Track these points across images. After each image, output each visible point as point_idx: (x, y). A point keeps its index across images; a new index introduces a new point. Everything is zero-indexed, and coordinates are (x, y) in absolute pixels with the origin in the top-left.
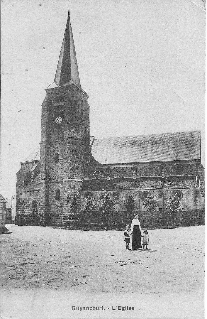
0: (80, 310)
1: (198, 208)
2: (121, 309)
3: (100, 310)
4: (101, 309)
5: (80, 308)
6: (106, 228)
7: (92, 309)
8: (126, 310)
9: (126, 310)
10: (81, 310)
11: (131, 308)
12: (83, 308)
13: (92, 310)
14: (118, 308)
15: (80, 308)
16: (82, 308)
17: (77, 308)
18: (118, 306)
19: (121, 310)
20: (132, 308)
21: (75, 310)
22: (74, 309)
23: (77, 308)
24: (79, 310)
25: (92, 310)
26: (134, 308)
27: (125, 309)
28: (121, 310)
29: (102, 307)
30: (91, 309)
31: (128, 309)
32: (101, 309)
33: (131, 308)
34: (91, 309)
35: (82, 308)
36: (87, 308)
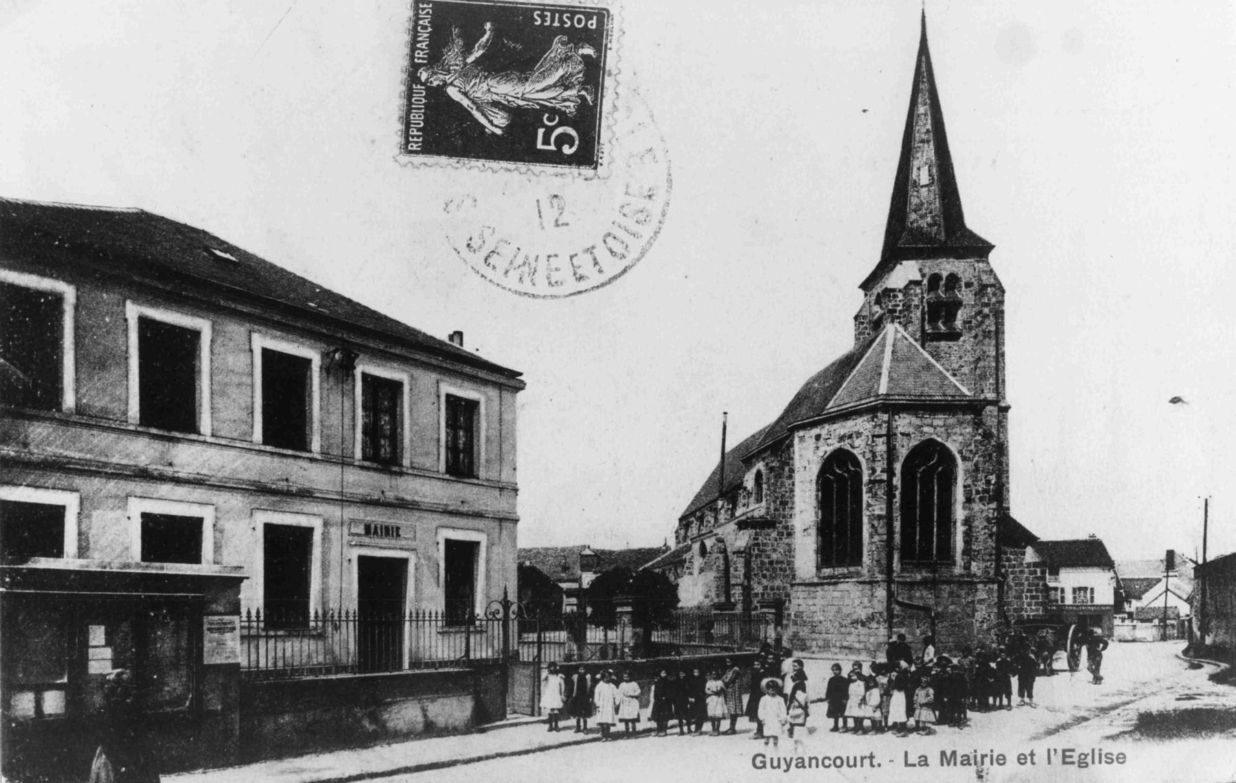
0: (784, 767)
1: (340, 386)
2: (1075, 759)
3: (862, 766)
4: (867, 762)
5: (785, 759)
6: (1098, 659)
7: (832, 762)
8: (1093, 763)
9: (1093, 763)
10: (789, 766)
11: (1114, 757)
12: (794, 762)
13: (830, 765)
14: (1064, 757)
15: (785, 759)
16: (791, 759)
17: (772, 759)
18: (1064, 751)
19: (1073, 763)
20: (1118, 758)
21: (764, 766)
22: (762, 765)
23: (772, 759)
24: (779, 766)
25: (830, 765)
26: (1004, 758)
27: (1089, 759)
28: (1073, 763)
29: (872, 757)
30: (827, 762)
31: (1104, 759)
32: (867, 762)
33: (1114, 757)
34: (827, 762)
35: (791, 759)
36: (810, 759)
